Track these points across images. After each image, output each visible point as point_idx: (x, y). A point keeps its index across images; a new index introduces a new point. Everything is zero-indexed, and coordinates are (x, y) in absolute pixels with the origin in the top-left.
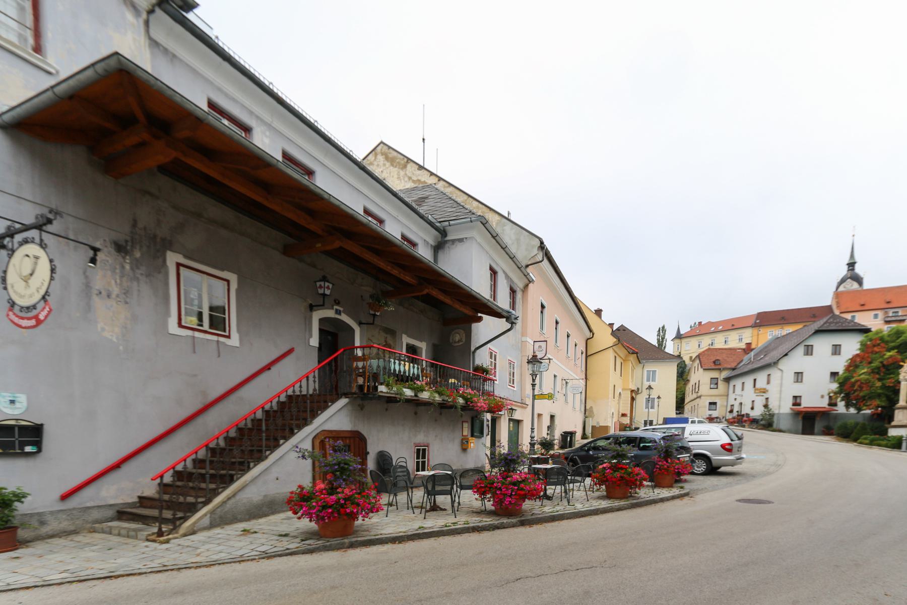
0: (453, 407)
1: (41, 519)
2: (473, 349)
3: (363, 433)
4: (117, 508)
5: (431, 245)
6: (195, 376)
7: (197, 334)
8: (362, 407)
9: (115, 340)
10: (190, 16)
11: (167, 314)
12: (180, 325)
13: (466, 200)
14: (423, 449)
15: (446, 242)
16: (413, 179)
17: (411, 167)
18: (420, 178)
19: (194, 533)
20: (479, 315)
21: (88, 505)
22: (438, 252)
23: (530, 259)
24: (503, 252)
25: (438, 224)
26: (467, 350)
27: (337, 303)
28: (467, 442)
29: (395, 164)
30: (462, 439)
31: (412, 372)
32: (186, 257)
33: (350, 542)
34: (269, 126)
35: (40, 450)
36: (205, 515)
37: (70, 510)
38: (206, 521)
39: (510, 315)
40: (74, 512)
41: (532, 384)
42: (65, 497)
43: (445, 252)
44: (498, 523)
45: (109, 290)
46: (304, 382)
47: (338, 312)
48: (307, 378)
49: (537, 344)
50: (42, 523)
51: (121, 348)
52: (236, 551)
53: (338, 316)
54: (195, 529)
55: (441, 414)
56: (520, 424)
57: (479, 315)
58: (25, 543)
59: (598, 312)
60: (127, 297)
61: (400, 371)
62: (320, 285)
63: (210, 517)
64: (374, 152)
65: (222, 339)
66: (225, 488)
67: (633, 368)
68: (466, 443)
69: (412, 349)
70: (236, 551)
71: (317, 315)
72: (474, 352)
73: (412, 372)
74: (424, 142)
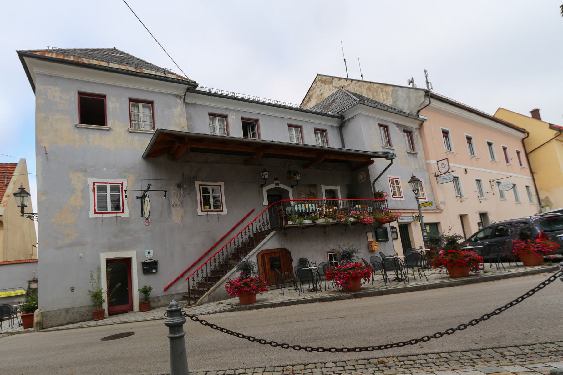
0: (345, 225)
1: (158, 298)
2: (372, 182)
3: (288, 249)
4: (183, 295)
5: (337, 127)
6: (210, 232)
7: (209, 213)
8: (285, 234)
9: (179, 223)
10: (198, 89)
12: (202, 211)
13: (369, 86)
14: (334, 254)
15: (345, 122)
16: (337, 87)
17: (335, 81)
18: (341, 85)
19: (201, 304)
20: (372, 159)
21: (173, 293)
22: (342, 129)
23: (420, 106)
24: (388, 112)
25: (337, 114)
26: (368, 184)
27: (276, 179)
28: (371, 246)
29: (326, 83)
30: (368, 245)
32: (202, 181)
33: (249, 306)
34: (235, 111)
35: (157, 271)
36: (206, 296)
37: (167, 295)
38: (207, 299)
39: (388, 155)
40: (169, 296)
41: (415, 197)
42: (166, 290)
43: (346, 128)
44: (336, 296)
45: (176, 204)
46: (251, 226)
48: (252, 223)
49: (440, 163)
50: (159, 301)
51: (181, 226)
54: (202, 302)
55: (346, 230)
56: (438, 225)
57: (372, 159)
58: (153, 308)
59: (536, 114)
60: (182, 204)
61: (302, 210)
62: (266, 173)
63: (208, 297)
64: (315, 82)
65: (219, 213)
66: (215, 283)
68: (371, 247)
69: (332, 194)
71: (265, 190)
74: (345, 61)
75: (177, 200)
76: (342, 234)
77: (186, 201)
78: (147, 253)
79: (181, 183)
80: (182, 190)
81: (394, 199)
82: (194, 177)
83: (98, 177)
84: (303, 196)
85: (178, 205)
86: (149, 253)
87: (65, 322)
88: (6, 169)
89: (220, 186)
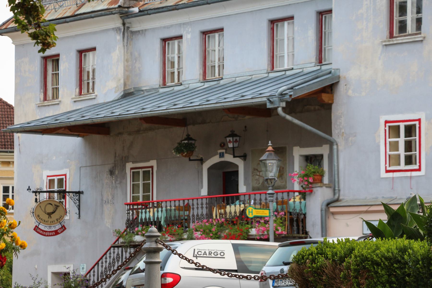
9: (110, 227)
31: (156, 216)
32: (133, 162)
47: (222, 155)
52: (391, 201)
53: (222, 159)
62: (230, 140)
70: (391, 201)
73: (156, 216)
75: (109, 193)
77: (117, 194)
78: (81, 270)
79: (113, 167)
80: (114, 179)
81: (390, 175)
82: (125, 157)
83: (50, 169)
85: (109, 202)
86: (83, 268)
88: (121, 105)
89: (152, 167)
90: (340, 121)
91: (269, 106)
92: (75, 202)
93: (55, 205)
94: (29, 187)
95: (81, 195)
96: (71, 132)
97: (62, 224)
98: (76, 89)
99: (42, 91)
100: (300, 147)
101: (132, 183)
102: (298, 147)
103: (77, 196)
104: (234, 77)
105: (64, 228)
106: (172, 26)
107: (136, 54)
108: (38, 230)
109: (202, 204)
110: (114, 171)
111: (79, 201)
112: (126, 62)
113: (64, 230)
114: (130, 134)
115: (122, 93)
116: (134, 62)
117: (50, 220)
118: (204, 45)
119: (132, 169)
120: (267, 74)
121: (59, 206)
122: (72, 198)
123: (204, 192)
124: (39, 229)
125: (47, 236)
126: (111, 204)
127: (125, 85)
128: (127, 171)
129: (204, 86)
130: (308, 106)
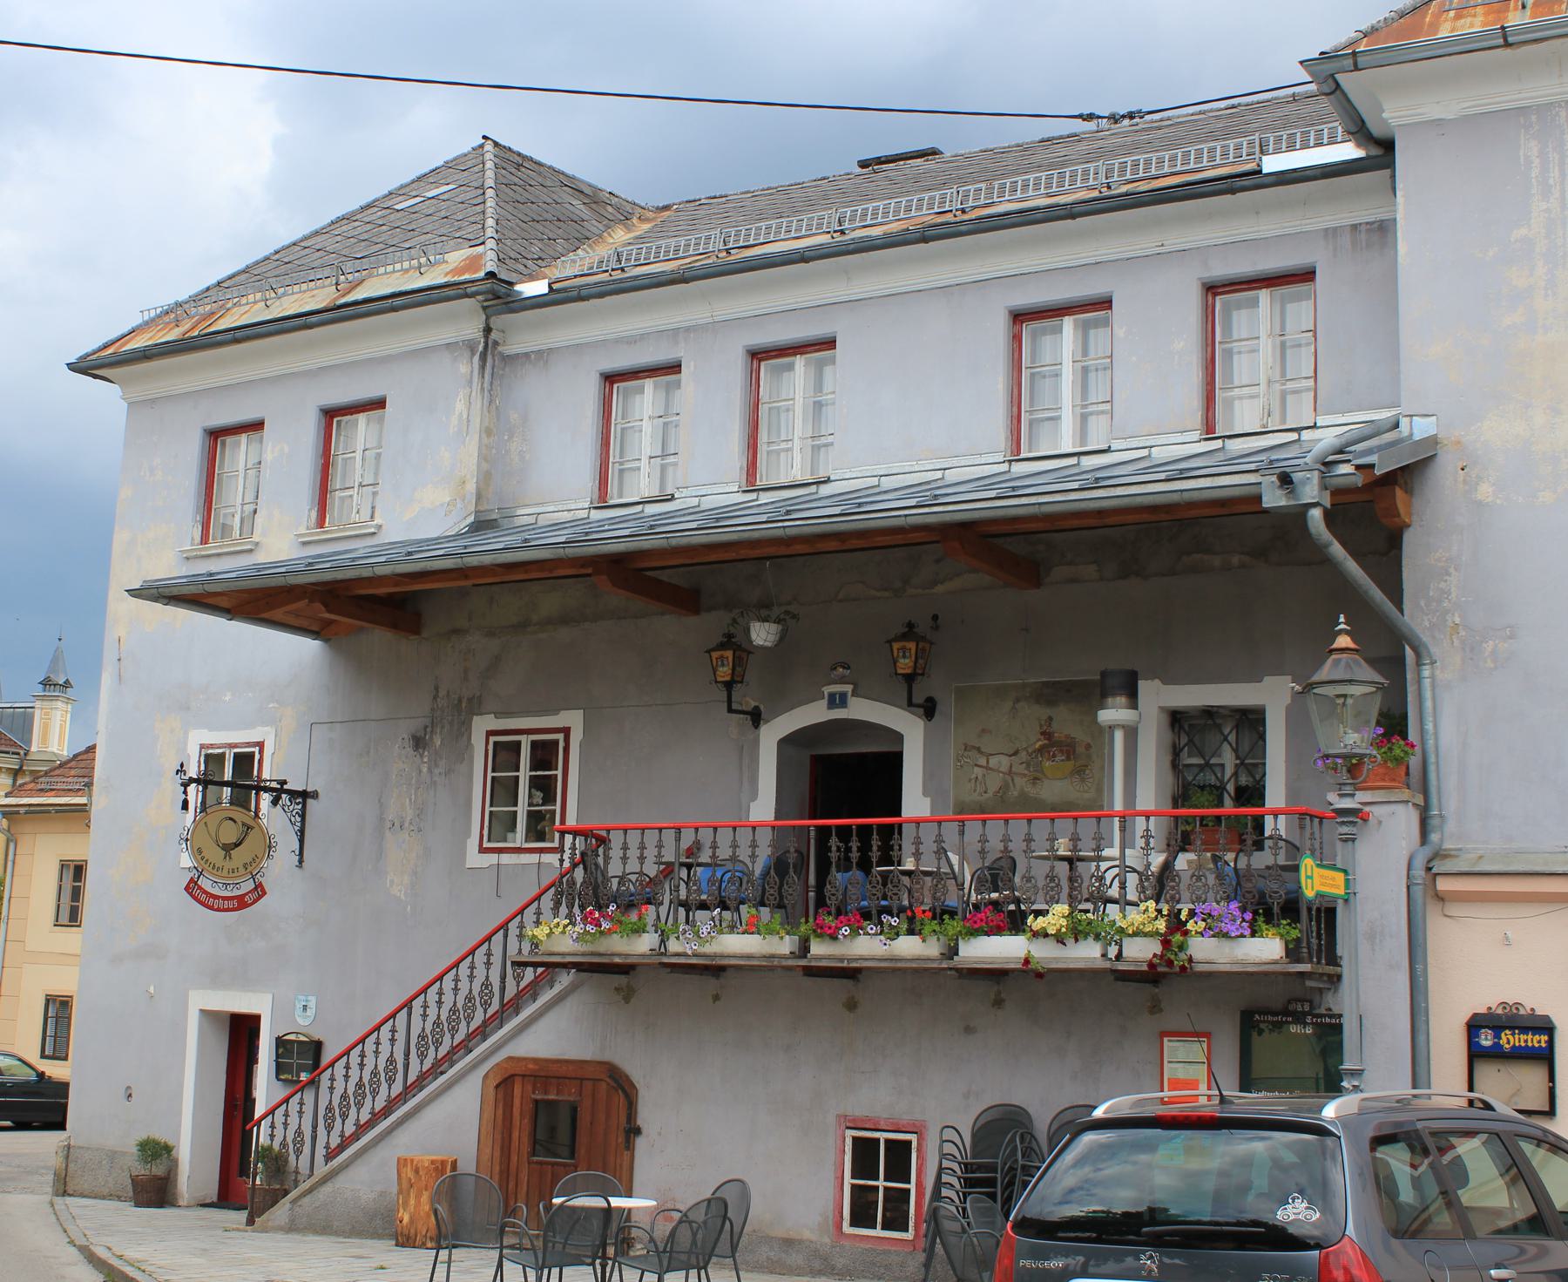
7: (506, 859)
9: (403, 897)
11: (468, 834)
32: (498, 715)
67: (1019, 1177)
72: (1331, 651)
75: (408, 800)
76: (969, 1030)
79: (426, 727)
80: (425, 760)
82: (470, 700)
83: (211, 728)
84: (993, 761)
85: (407, 825)
86: (305, 1007)
87: (106, 1191)
89: (566, 731)
90: (1442, 585)
91: (1274, 498)
92: (293, 819)
93: (244, 824)
94: (182, 765)
95: (310, 802)
96: (329, 611)
97: (257, 880)
98: (310, 510)
99: (198, 519)
100: (1164, 683)
101: (490, 775)
102: (1157, 682)
103: (298, 804)
104: (876, 474)
105: (259, 891)
106: (643, 337)
107: (514, 416)
108: (197, 892)
109: (642, 847)
110: (427, 737)
111: (303, 816)
112: (484, 436)
113: (260, 897)
114: (491, 633)
115: (471, 519)
116: (506, 437)
117: (228, 865)
118: (753, 387)
119: (490, 733)
120: (1007, 464)
121: (252, 828)
122: (286, 808)
123: (763, 808)
124: (200, 888)
125: (218, 910)
126: (412, 833)
127: (479, 497)
128: (473, 741)
129: (757, 500)
130: (1197, 556)
